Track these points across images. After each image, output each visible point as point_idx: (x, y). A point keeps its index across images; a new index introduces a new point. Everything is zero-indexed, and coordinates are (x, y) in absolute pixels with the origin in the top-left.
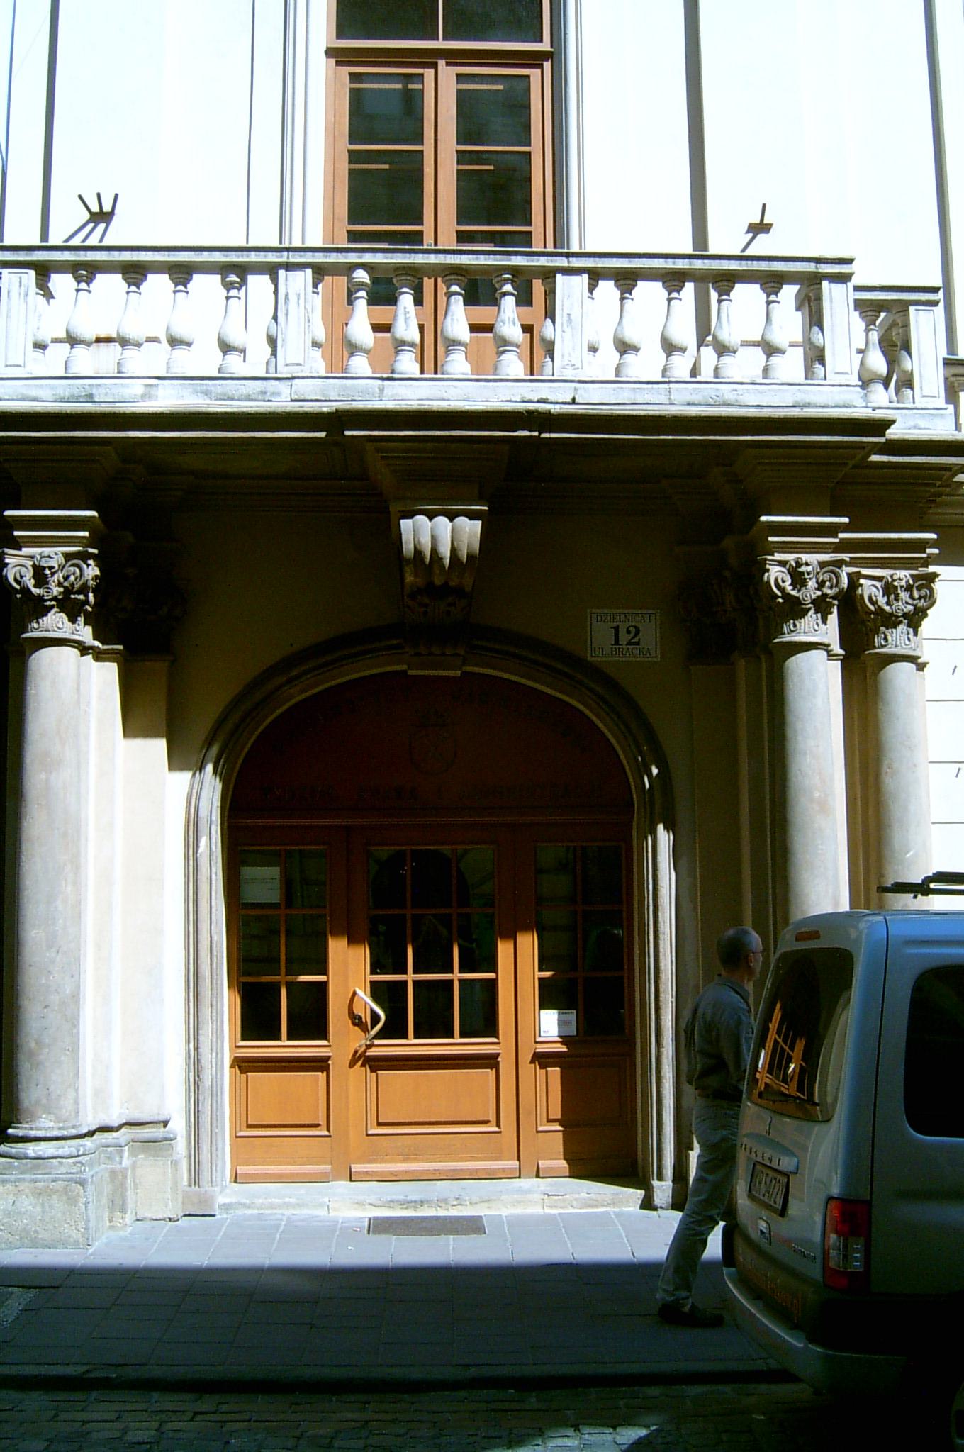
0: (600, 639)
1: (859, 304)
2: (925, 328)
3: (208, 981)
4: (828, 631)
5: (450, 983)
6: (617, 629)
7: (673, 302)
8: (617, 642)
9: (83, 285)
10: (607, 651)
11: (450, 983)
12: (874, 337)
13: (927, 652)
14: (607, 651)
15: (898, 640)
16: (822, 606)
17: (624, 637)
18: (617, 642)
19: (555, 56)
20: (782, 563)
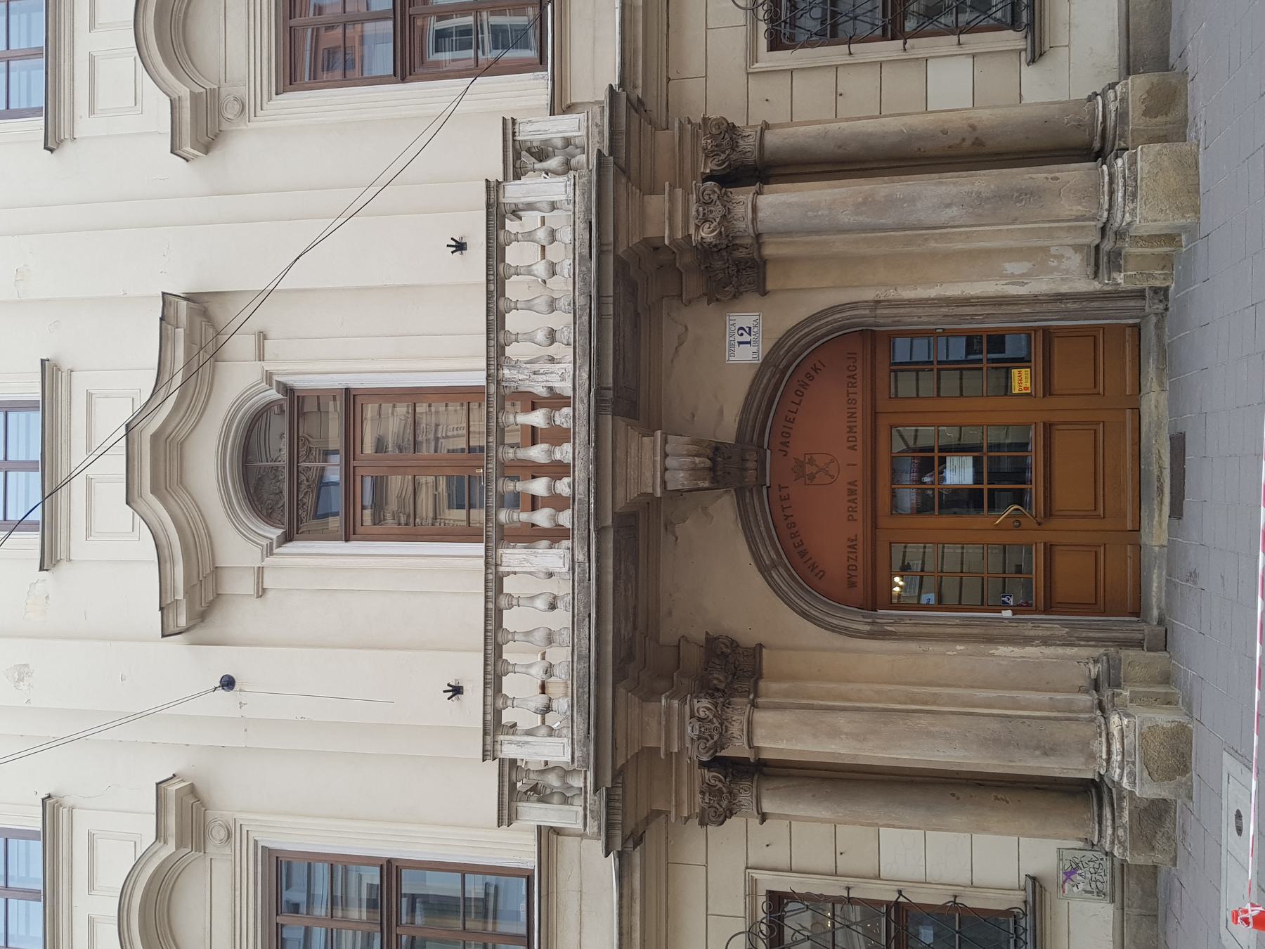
0: (748, 355)
1: (517, 177)
2: (530, 132)
3: (907, 119)
4: (742, 197)
5: (989, 490)
6: (740, 343)
7: (1015, 57)
8: (749, 343)
9: (509, 703)
10: (755, 349)
11: (989, 490)
12: (538, 165)
13: (756, 121)
14: (755, 349)
15: (748, 144)
16: (726, 202)
17: (746, 338)
18: (749, 343)
19: (350, 398)
20: (698, 227)
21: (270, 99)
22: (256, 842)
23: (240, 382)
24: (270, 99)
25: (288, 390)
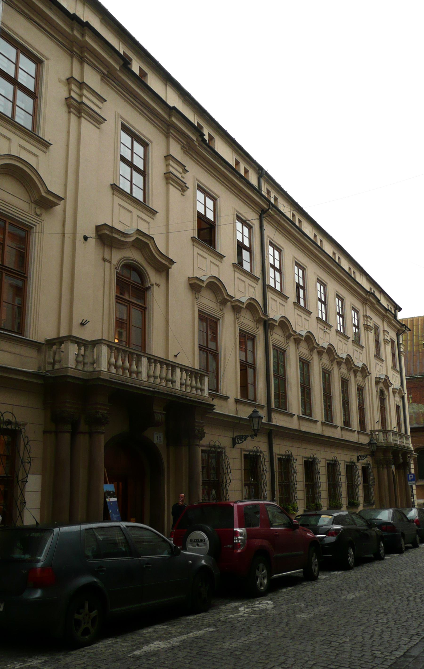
17: (159, 439)
21: (198, 307)
22: (221, 318)
23: (153, 277)
24: (198, 307)
25: (149, 288)
